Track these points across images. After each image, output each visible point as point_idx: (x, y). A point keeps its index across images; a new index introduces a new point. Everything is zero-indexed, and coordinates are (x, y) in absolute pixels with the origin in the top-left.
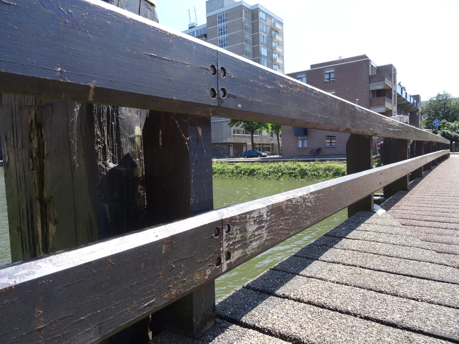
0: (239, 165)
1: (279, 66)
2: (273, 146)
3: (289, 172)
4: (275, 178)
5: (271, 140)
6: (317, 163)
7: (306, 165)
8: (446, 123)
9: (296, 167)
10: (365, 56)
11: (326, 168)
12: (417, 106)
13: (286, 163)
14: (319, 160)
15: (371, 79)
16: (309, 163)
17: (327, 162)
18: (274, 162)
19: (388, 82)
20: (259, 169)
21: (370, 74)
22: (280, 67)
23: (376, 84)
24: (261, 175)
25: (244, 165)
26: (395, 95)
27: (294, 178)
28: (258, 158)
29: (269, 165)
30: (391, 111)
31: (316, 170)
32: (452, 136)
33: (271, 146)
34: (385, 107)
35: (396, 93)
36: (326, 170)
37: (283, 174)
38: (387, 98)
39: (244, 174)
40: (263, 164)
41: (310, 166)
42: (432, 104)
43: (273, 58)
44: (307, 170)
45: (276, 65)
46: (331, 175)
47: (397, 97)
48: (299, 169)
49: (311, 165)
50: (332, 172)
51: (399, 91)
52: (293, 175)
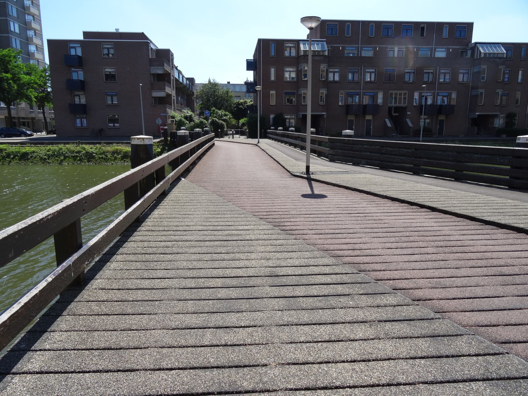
0: (4, 148)
1: (33, 17)
2: (34, 121)
3: (73, 155)
4: (56, 162)
5: (31, 112)
6: (103, 146)
7: (91, 148)
8: (215, 110)
9: (80, 150)
10: (142, 36)
11: (114, 151)
12: (192, 89)
13: (67, 146)
14: (104, 143)
15: (152, 62)
16: (95, 146)
17: (114, 145)
18: (52, 144)
19: (167, 68)
20: (34, 152)
21: (150, 57)
22: (35, 19)
23: (156, 68)
24: (38, 158)
25: (11, 148)
26: (173, 80)
27: (79, 162)
28: (23, 139)
29: (46, 147)
30: (171, 95)
31: (104, 153)
32: (219, 124)
33: (31, 121)
34: (165, 92)
35: (174, 78)
36: (113, 153)
37: (65, 157)
38: (167, 83)
39: (13, 159)
40: (38, 146)
41: (96, 149)
42: (205, 90)
43: (25, 5)
44: (94, 153)
45: (29, 15)
46: (119, 158)
47: (175, 80)
48: (84, 152)
49: (97, 147)
50: (120, 155)
51: (176, 76)
52: (78, 158)
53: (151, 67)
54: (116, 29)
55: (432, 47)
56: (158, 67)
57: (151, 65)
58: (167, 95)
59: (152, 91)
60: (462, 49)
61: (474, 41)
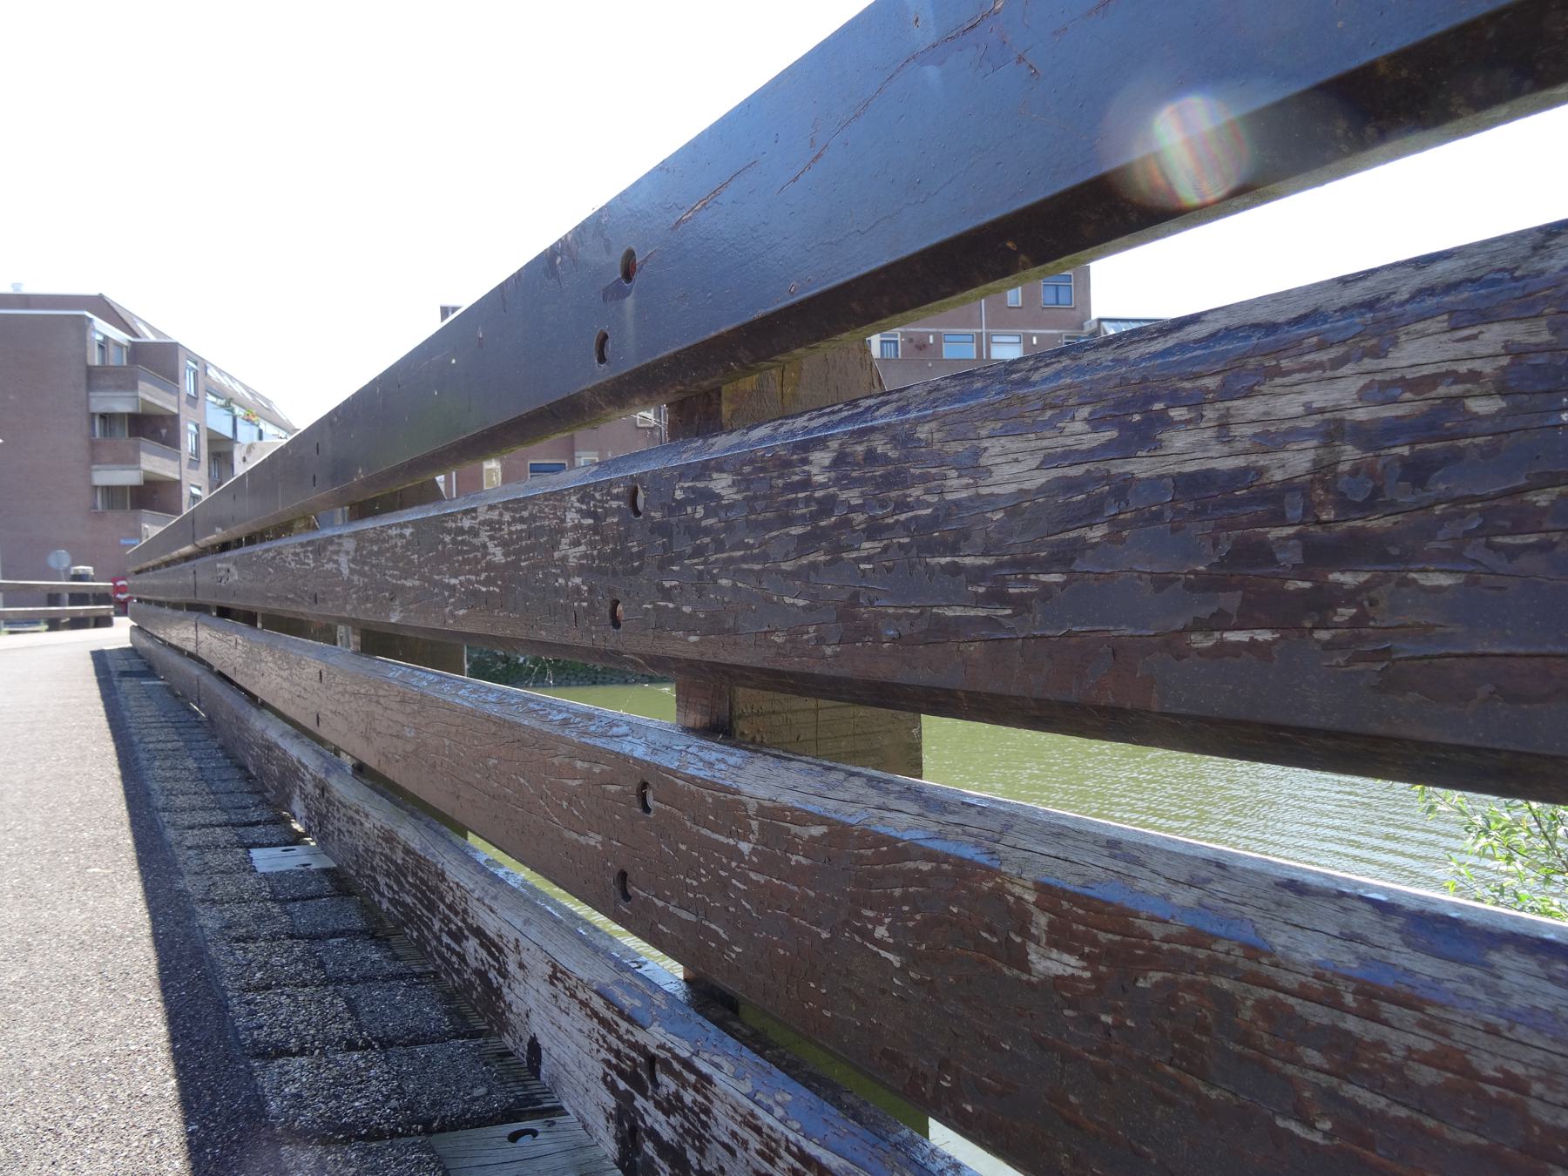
30: (177, 483)
34: (139, 469)
53: (91, 394)
54: (14, 285)
55: (979, 331)
56: (118, 394)
57: (90, 387)
58: (145, 482)
59: (95, 467)
60: (1068, 337)
61: (1095, 315)
